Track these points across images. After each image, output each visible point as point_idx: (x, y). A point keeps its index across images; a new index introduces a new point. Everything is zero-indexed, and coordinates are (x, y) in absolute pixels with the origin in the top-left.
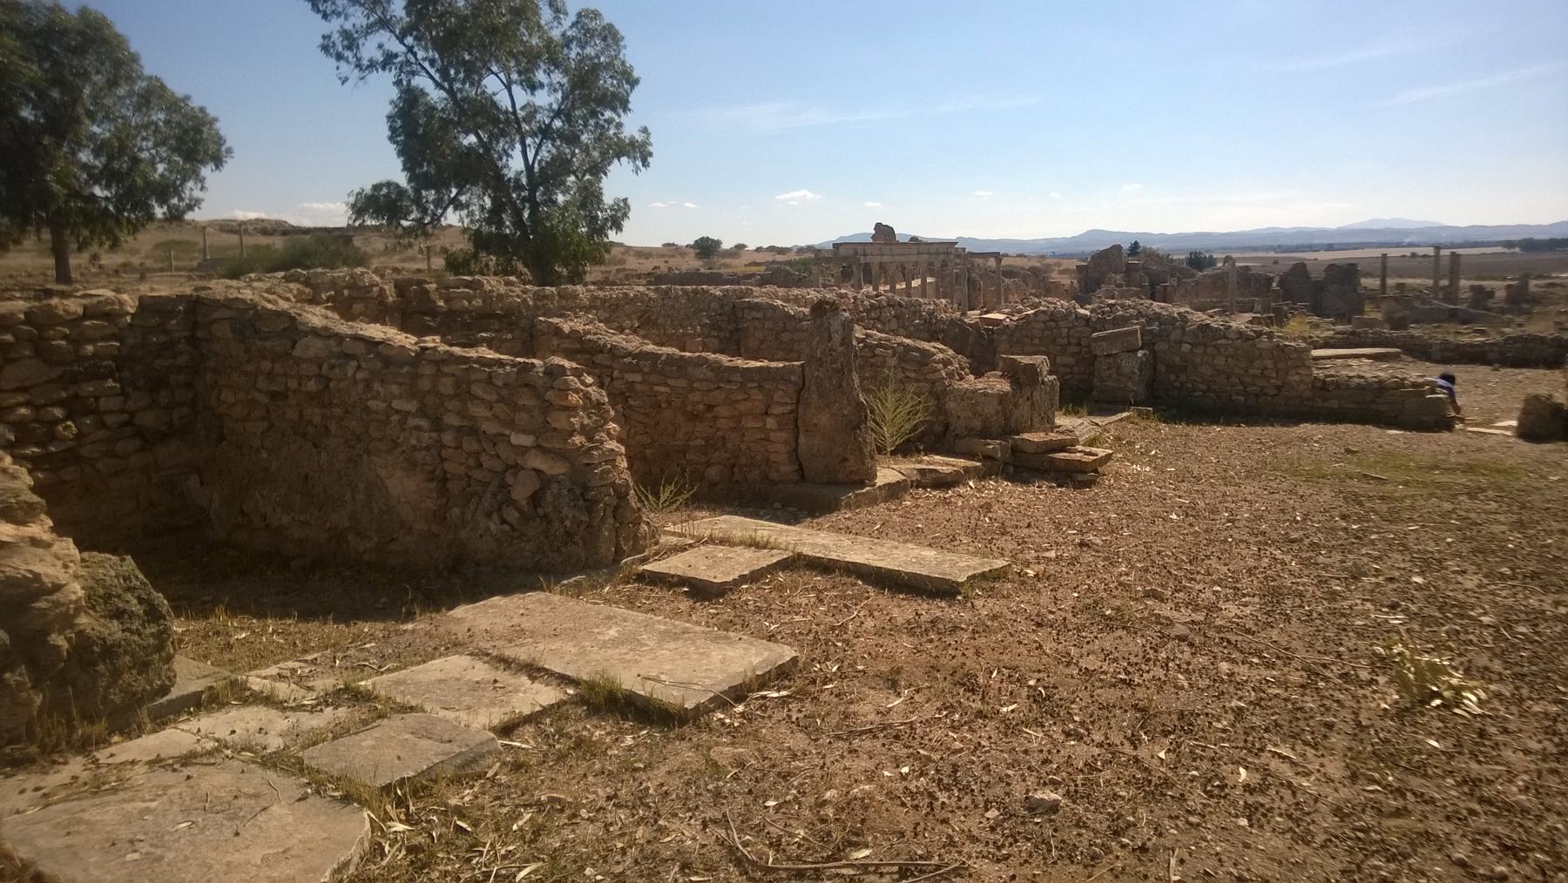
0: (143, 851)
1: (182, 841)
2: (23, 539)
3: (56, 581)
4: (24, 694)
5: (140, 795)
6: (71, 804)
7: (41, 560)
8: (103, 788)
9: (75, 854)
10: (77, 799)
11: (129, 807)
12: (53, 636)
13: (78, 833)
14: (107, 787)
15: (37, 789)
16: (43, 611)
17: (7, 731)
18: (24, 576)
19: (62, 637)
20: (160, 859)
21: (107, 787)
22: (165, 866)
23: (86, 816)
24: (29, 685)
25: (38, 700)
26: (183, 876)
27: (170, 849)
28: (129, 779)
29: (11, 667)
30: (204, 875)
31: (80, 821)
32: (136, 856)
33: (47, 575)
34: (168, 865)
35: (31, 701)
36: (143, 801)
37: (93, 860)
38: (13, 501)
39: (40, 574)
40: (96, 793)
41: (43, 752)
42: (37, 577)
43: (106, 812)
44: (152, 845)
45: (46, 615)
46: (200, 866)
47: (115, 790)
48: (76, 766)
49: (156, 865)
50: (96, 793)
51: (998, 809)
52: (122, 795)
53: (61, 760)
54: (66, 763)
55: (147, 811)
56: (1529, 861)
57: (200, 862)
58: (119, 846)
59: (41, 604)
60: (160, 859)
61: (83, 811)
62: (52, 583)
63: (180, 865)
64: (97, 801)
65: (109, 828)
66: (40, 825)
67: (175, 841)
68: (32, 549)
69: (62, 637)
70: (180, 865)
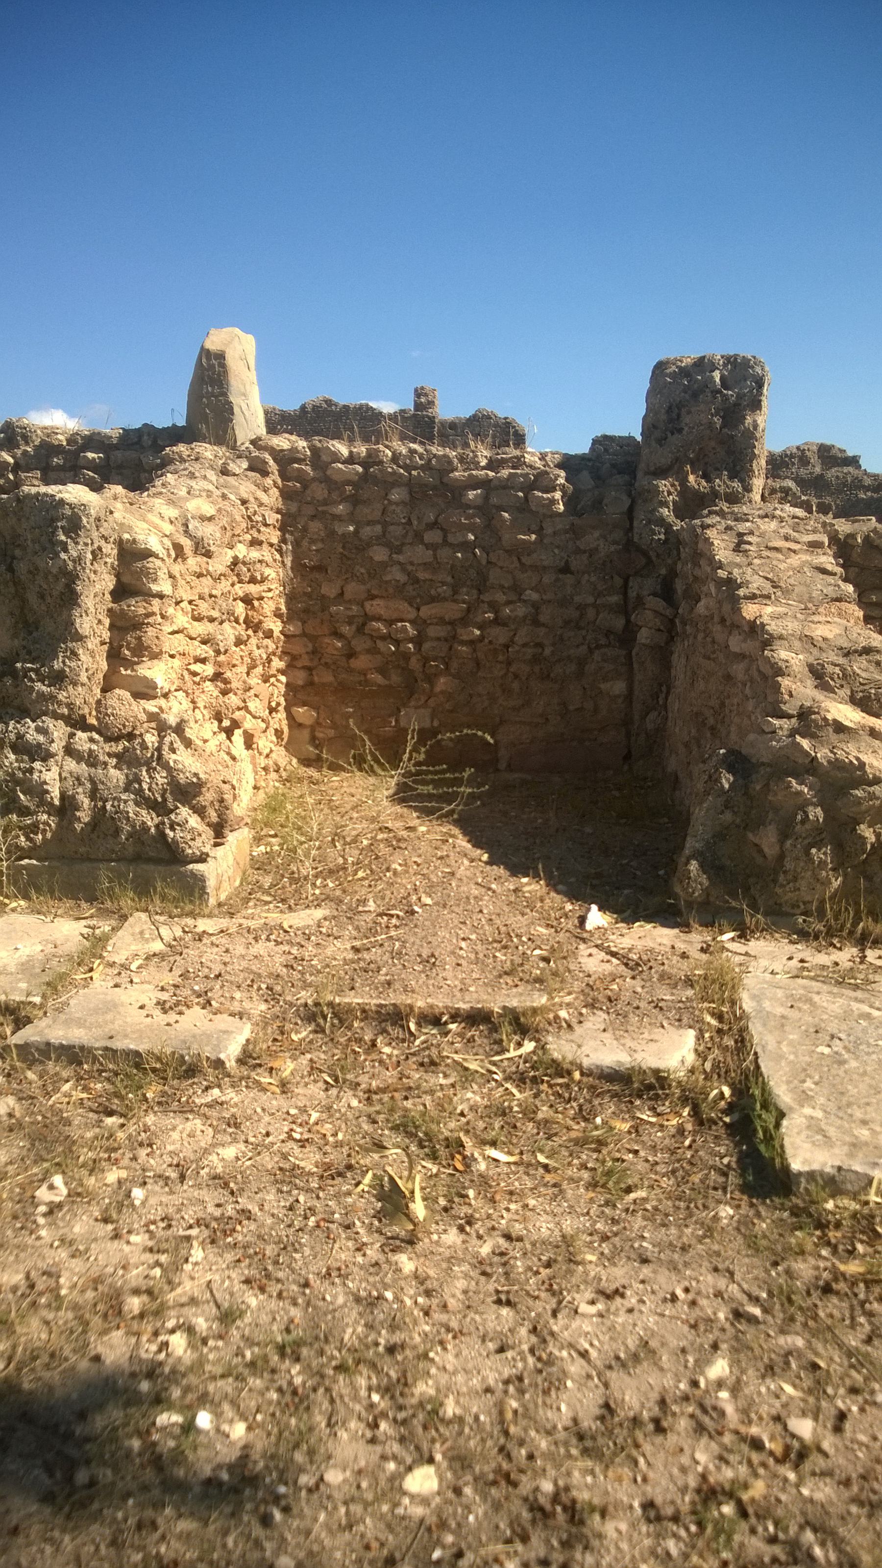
0: (836, 1049)
1: (874, 1057)
2: (863, 727)
3: (877, 774)
4: (824, 873)
5: (872, 999)
6: (814, 983)
7: (874, 752)
8: (847, 981)
9: (783, 1026)
10: (823, 982)
11: (855, 1006)
12: (862, 826)
13: (800, 1009)
14: (852, 981)
15: (802, 961)
16: (858, 801)
17: (804, 903)
18: (851, 762)
19: (871, 830)
20: (842, 1063)
21: (852, 981)
22: (841, 1073)
23: (816, 998)
24: (830, 866)
25: (836, 883)
26: (850, 1087)
27: (857, 1058)
28: (875, 982)
29: (819, 845)
30: (868, 1097)
31: (810, 1001)
32: (827, 1050)
33: (871, 766)
34: (846, 1072)
35: (827, 883)
36: (871, 1007)
37: (791, 1037)
38: (873, 691)
39: (864, 764)
40: (840, 983)
41: (827, 933)
42: (862, 765)
43: (834, 1003)
44: (845, 1048)
45: (860, 803)
46: (870, 1086)
47: (856, 987)
48: (845, 956)
49: (835, 1066)
50: (840, 983)
51: (736, 1042)
52: (859, 994)
53: (838, 945)
54: (840, 949)
55: (867, 1016)
56: (114, 761)
57: (874, 1083)
58: (820, 1035)
59: (859, 793)
60: (842, 1063)
61: (818, 993)
62: (874, 775)
63: (855, 1076)
64: (835, 990)
65: (825, 1017)
66: (778, 990)
67: (868, 1054)
68: (869, 739)
69: (871, 830)
70: (855, 1076)
